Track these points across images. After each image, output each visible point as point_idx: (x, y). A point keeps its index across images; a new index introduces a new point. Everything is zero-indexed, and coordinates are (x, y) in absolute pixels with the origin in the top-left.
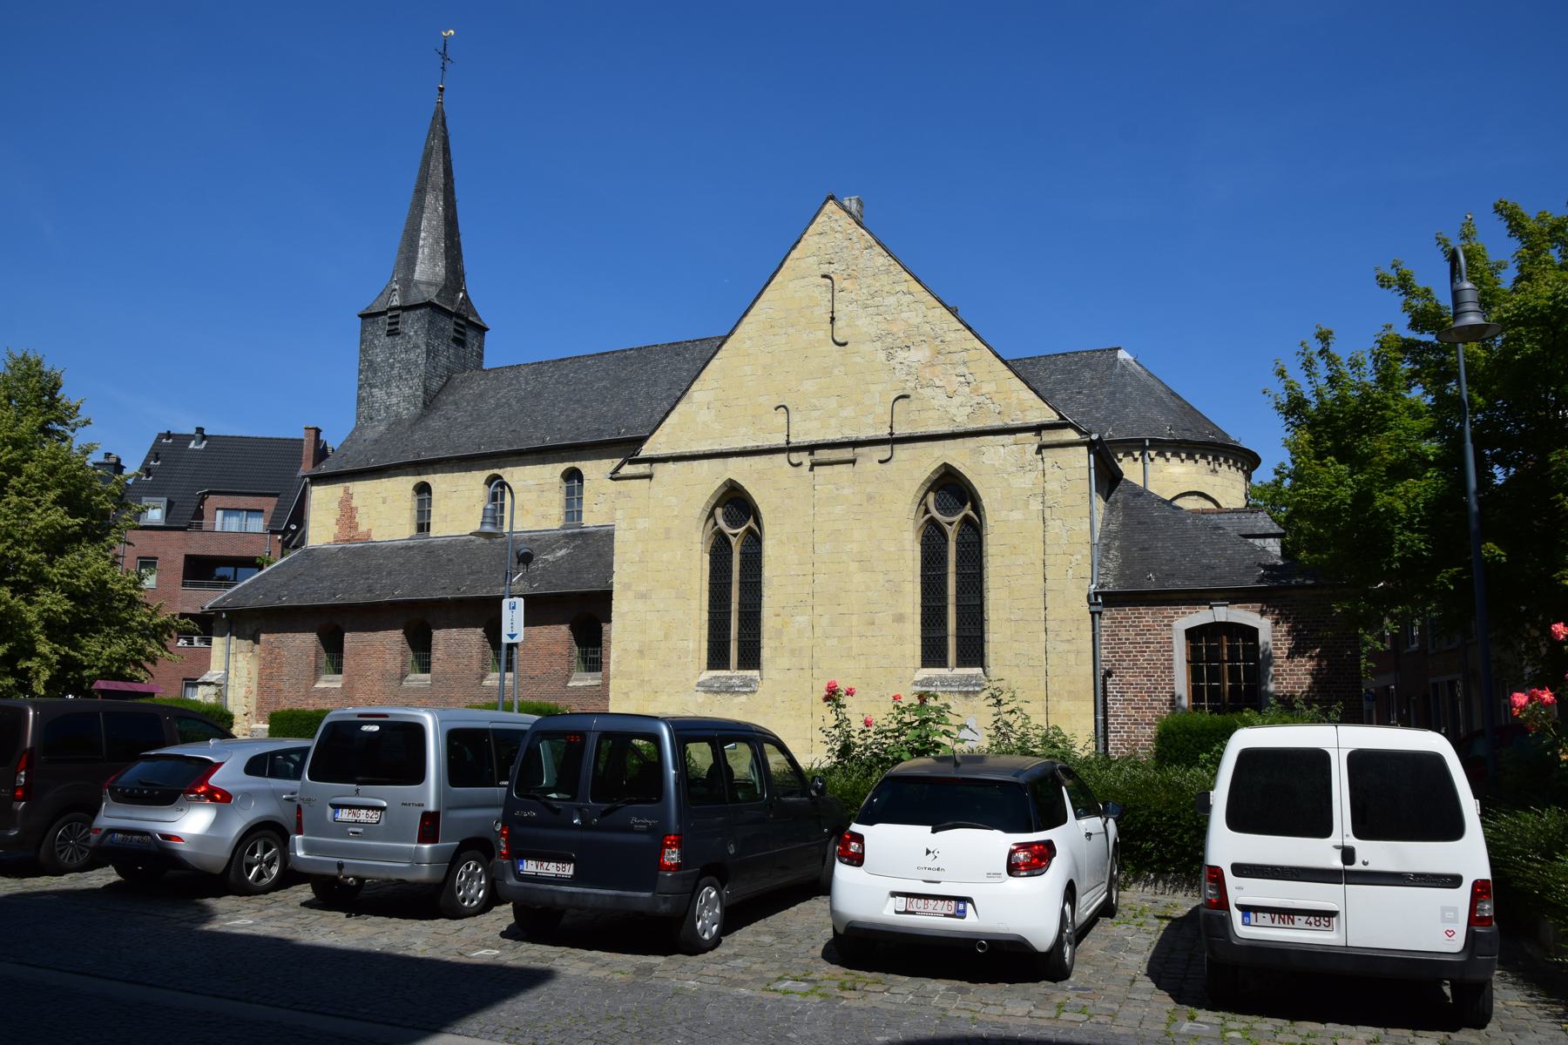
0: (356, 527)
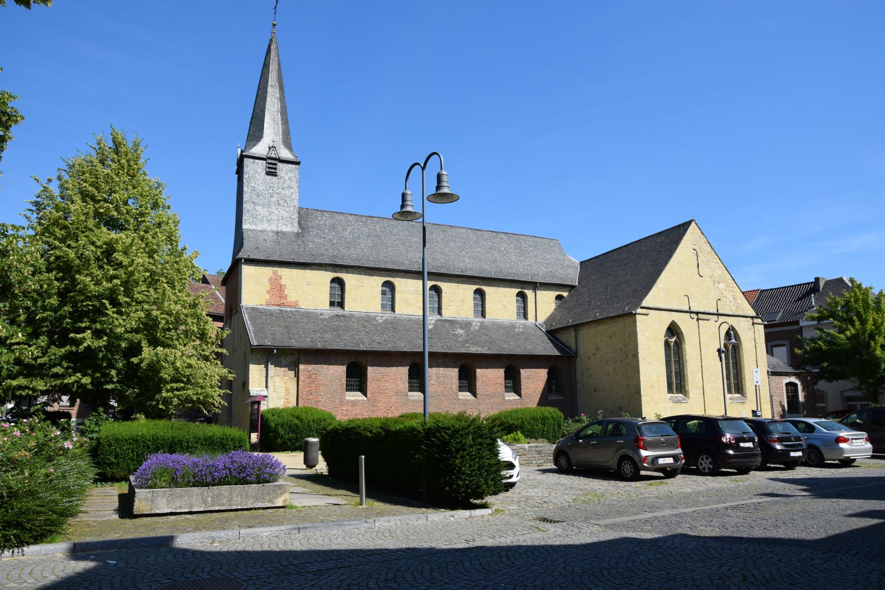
0: (286, 297)
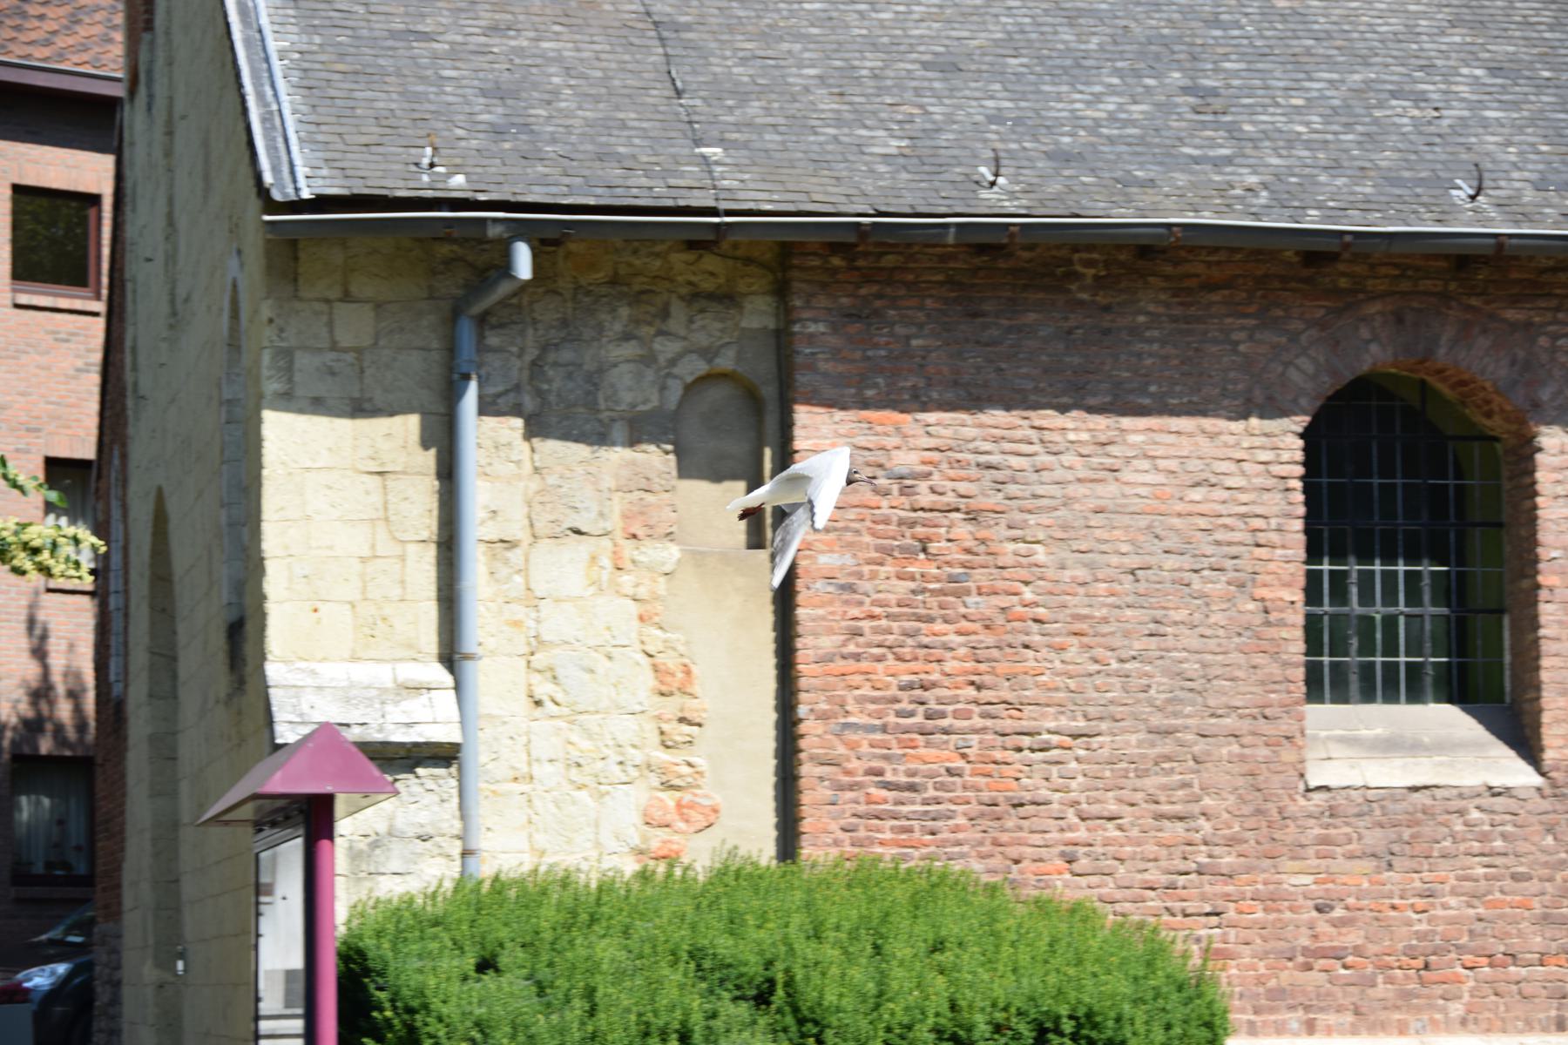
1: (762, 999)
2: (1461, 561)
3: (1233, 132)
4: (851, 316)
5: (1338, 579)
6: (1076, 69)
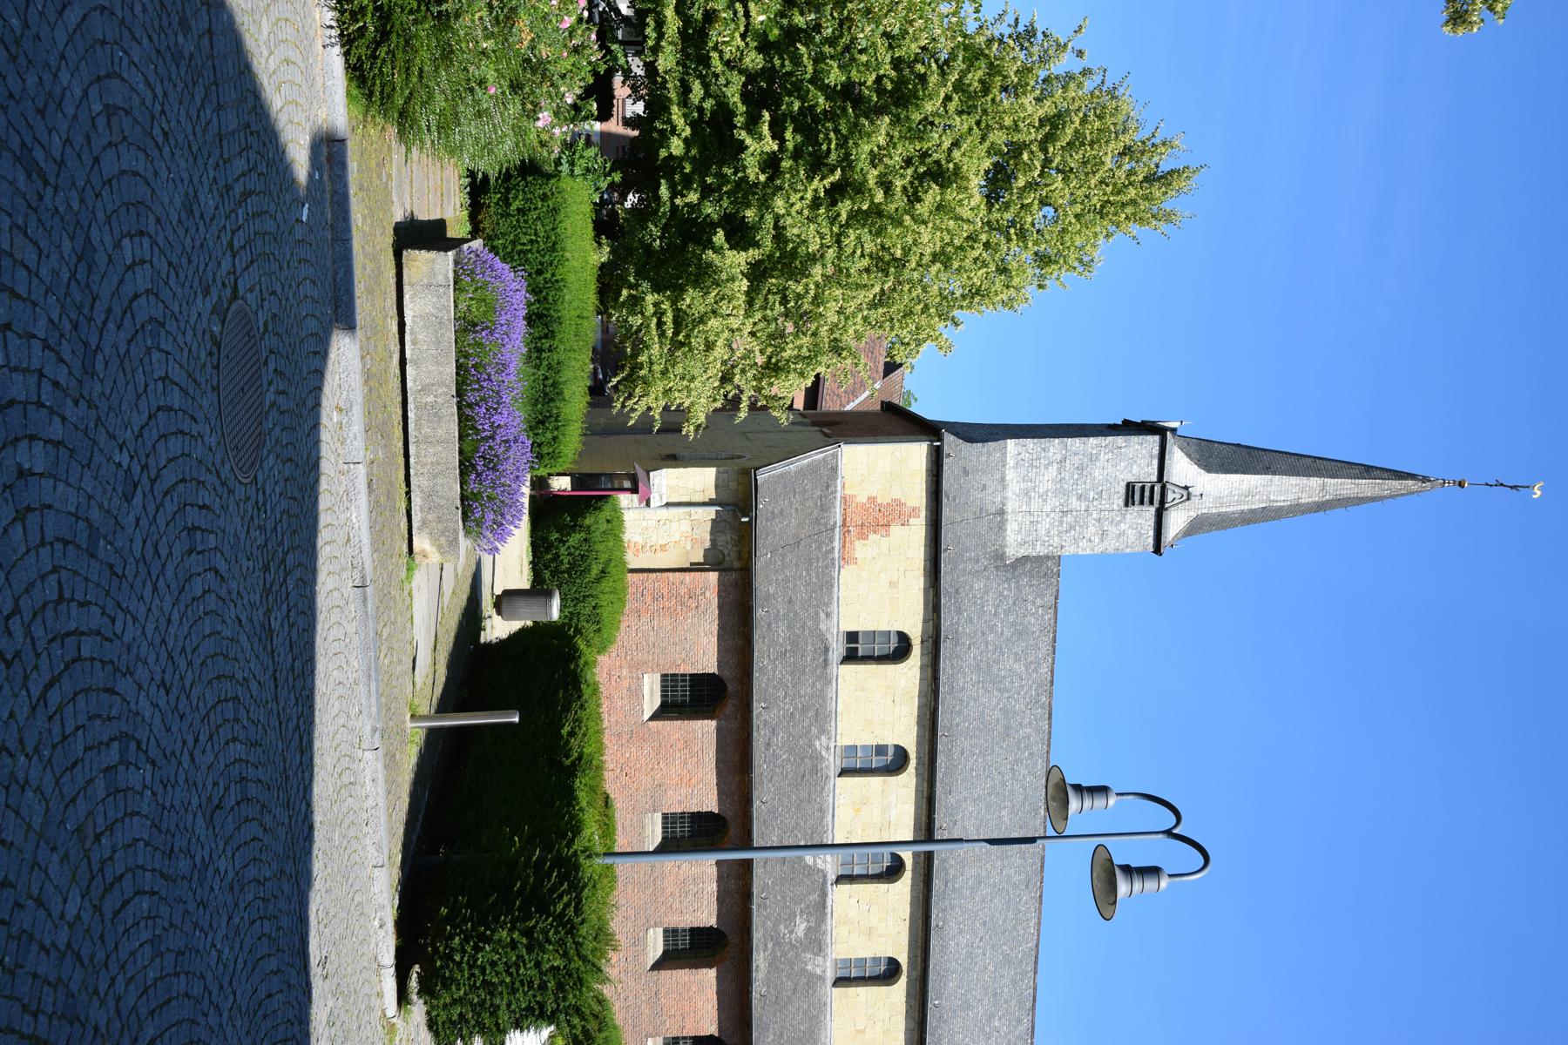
0: (863, 536)
1: (603, 572)
2: (691, 706)
3: (776, 659)
4: (736, 584)
5: (685, 681)
6: (790, 627)
